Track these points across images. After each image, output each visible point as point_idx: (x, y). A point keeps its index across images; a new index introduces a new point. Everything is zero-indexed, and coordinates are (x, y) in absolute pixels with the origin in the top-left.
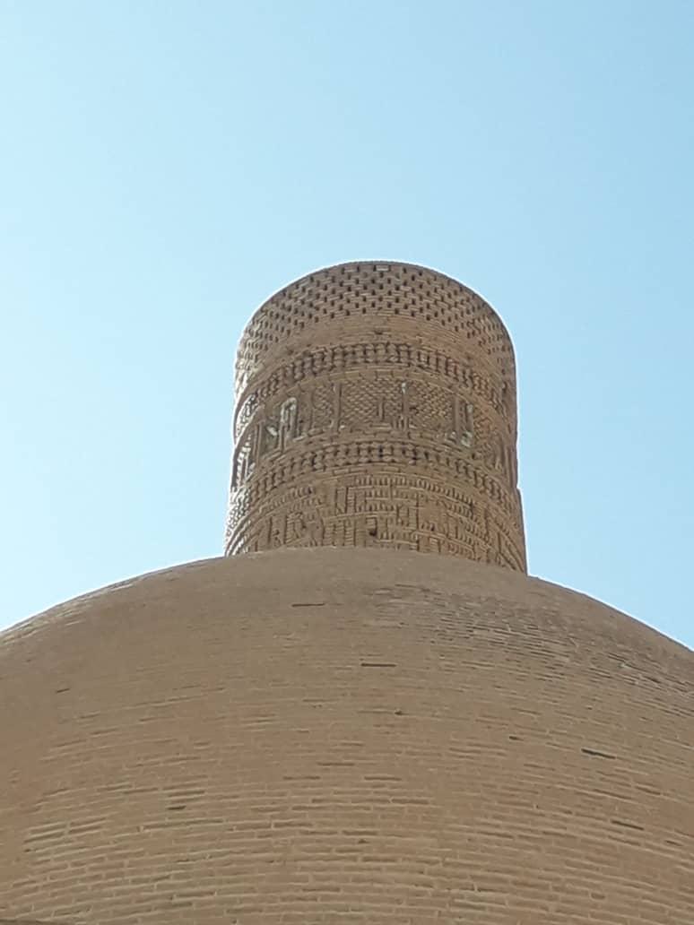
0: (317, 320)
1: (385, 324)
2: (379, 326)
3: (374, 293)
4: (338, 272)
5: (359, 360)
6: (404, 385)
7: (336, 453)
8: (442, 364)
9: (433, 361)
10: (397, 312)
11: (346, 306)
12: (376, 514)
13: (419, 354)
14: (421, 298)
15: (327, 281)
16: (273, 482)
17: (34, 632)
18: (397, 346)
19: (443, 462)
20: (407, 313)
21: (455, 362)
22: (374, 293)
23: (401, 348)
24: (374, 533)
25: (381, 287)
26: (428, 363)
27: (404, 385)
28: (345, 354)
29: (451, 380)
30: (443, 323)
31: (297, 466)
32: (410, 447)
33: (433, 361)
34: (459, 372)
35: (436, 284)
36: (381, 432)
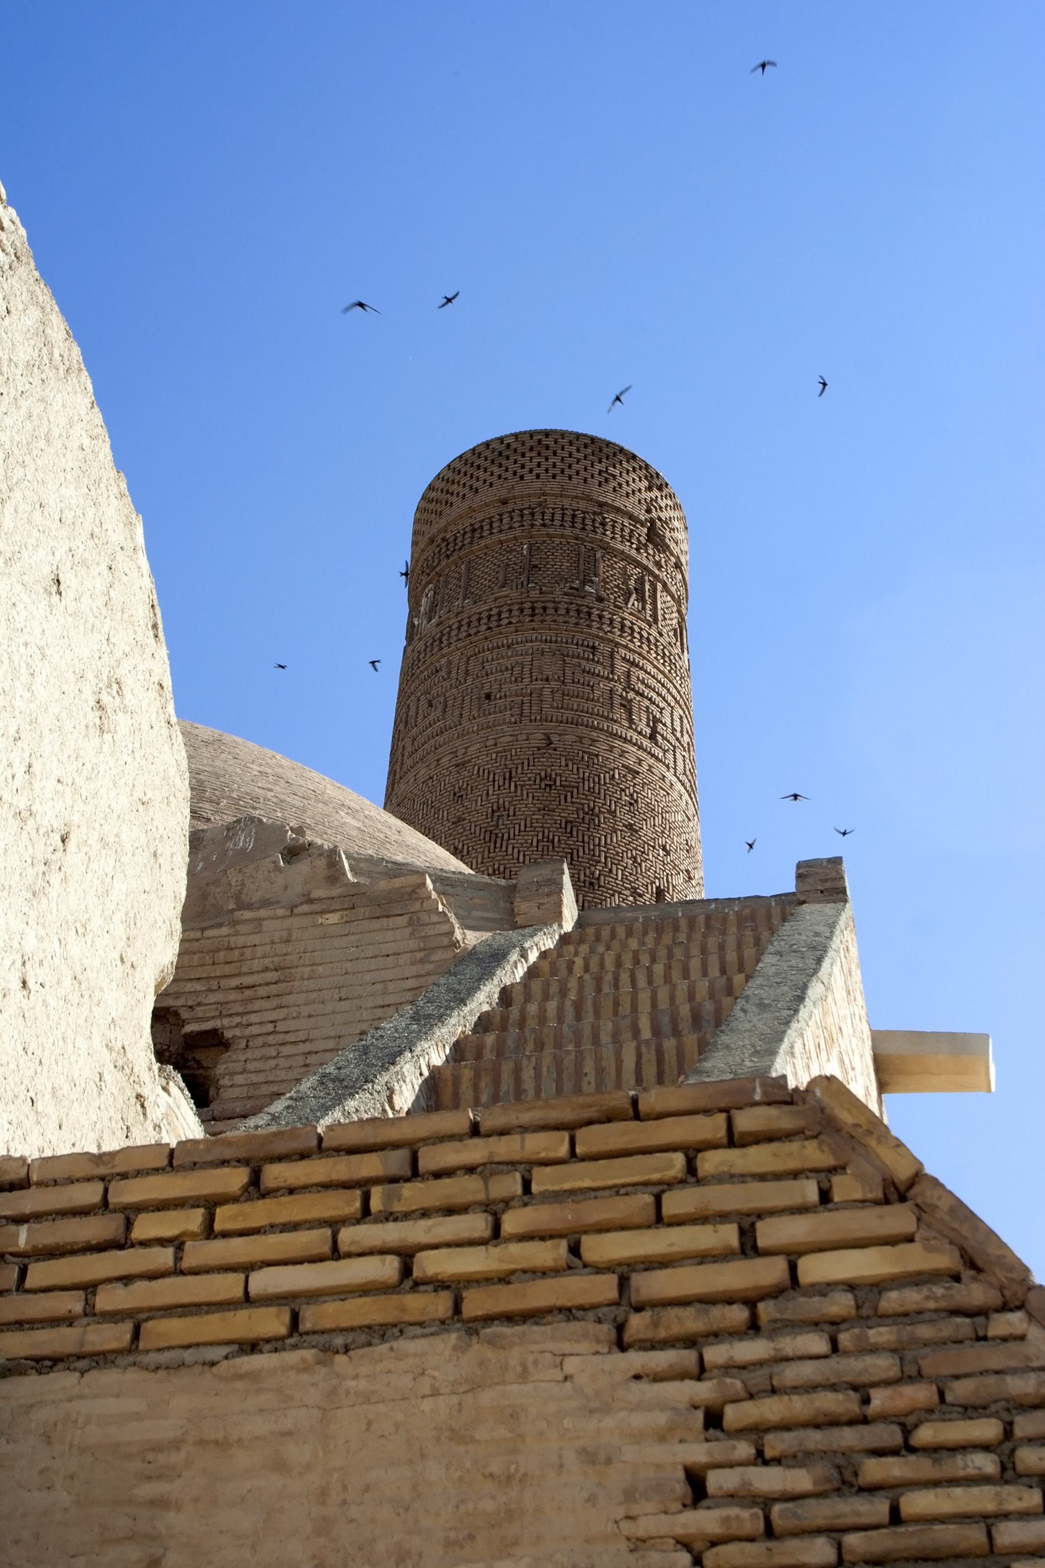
0: (491, 485)
1: (510, 493)
2: (504, 494)
3: (500, 466)
4: (527, 437)
5: (516, 525)
6: (525, 546)
7: (459, 628)
8: (568, 518)
9: (558, 517)
10: (538, 476)
11: (520, 472)
12: (492, 678)
13: (543, 513)
14: (547, 459)
15: (488, 453)
16: (432, 650)
17: (339, 785)
18: (521, 510)
19: (562, 612)
20: (533, 476)
21: (583, 512)
22: (500, 466)
23: (526, 512)
24: (488, 696)
25: (563, 448)
26: (553, 520)
27: (525, 546)
28: (474, 530)
29: (577, 531)
30: (570, 478)
31: (463, 629)
32: (527, 605)
33: (558, 517)
34: (588, 522)
35: (564, 442)
36: (500, 597)
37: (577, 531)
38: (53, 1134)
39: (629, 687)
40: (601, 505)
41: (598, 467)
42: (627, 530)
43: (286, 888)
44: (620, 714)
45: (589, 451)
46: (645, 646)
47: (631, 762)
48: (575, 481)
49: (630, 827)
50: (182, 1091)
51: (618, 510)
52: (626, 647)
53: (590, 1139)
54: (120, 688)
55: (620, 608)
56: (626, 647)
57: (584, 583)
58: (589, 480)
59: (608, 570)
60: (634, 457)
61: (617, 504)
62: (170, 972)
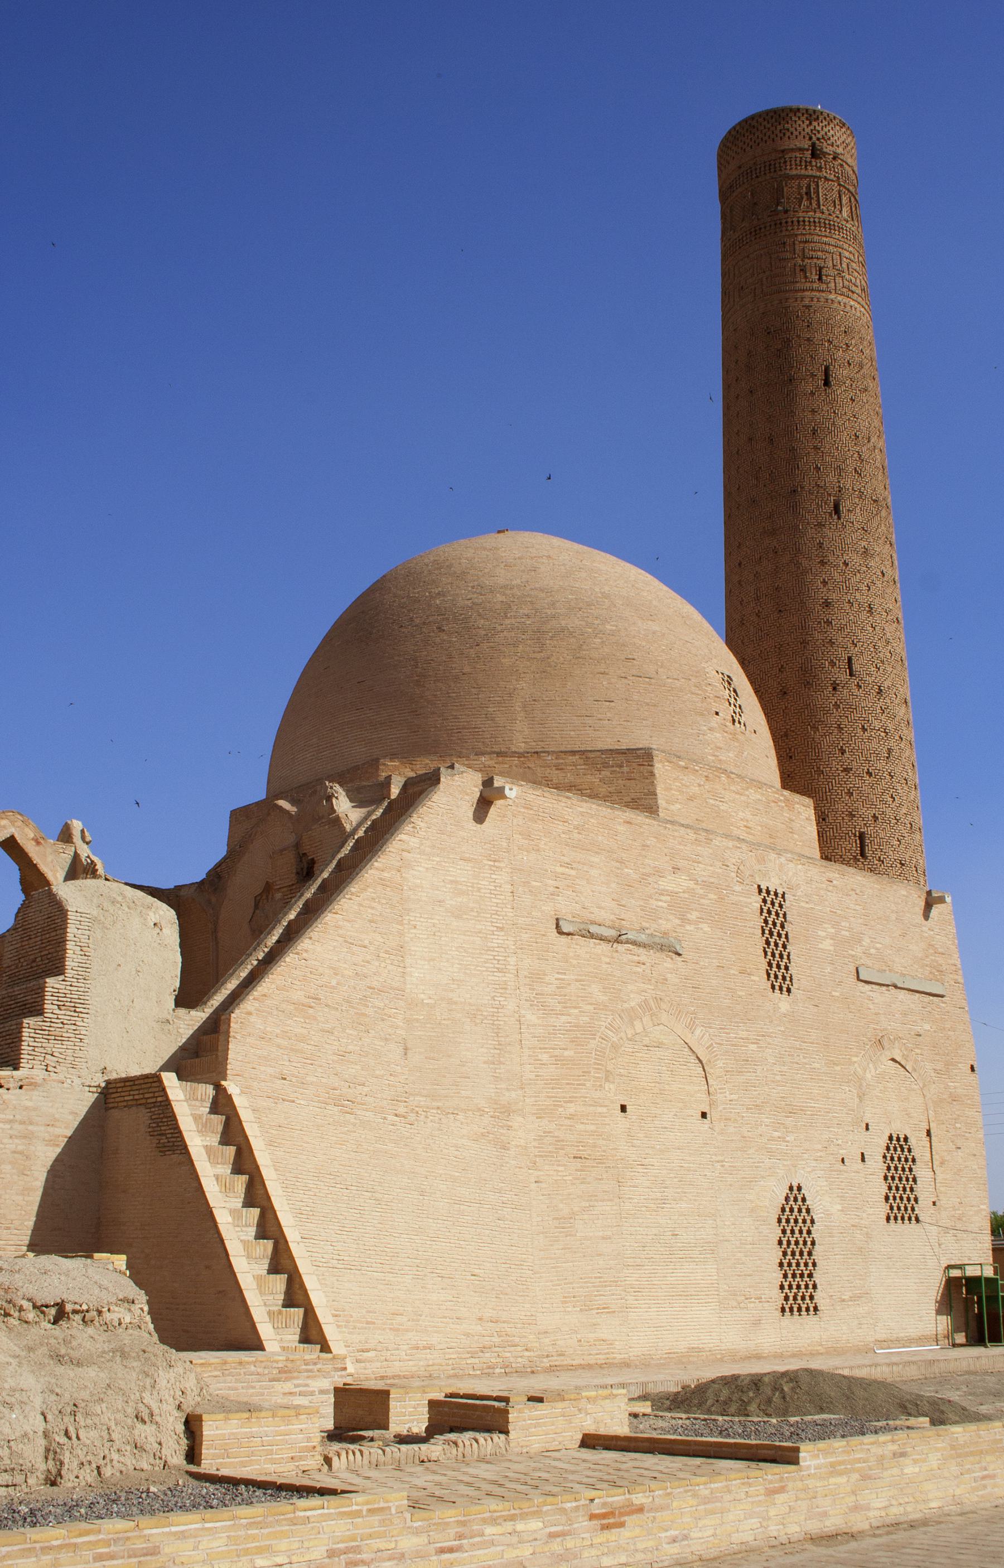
37: (772, 174)
38: (277, 1297)
39: (804, 258)
40: (783, 151)
41: (779, 128)
42: (798, 159)
43: (121, 1472)
44: (800, 276)
45: (774, 120)
46: (812, 228)
47: (807, 302)
48: (768, 143)
49: (808, 340)
50: (851, 1368)
51: (792, 150)
52: (802, 234)
53: (37, 1031)
54: (575, 786)
55: (797, 211)
56: (802, 234)
57: (777, 205)
58: (775, 139)
59: (790, 189)
60: (798, 110)
61: (792, 146)
62: (631, 1354)
